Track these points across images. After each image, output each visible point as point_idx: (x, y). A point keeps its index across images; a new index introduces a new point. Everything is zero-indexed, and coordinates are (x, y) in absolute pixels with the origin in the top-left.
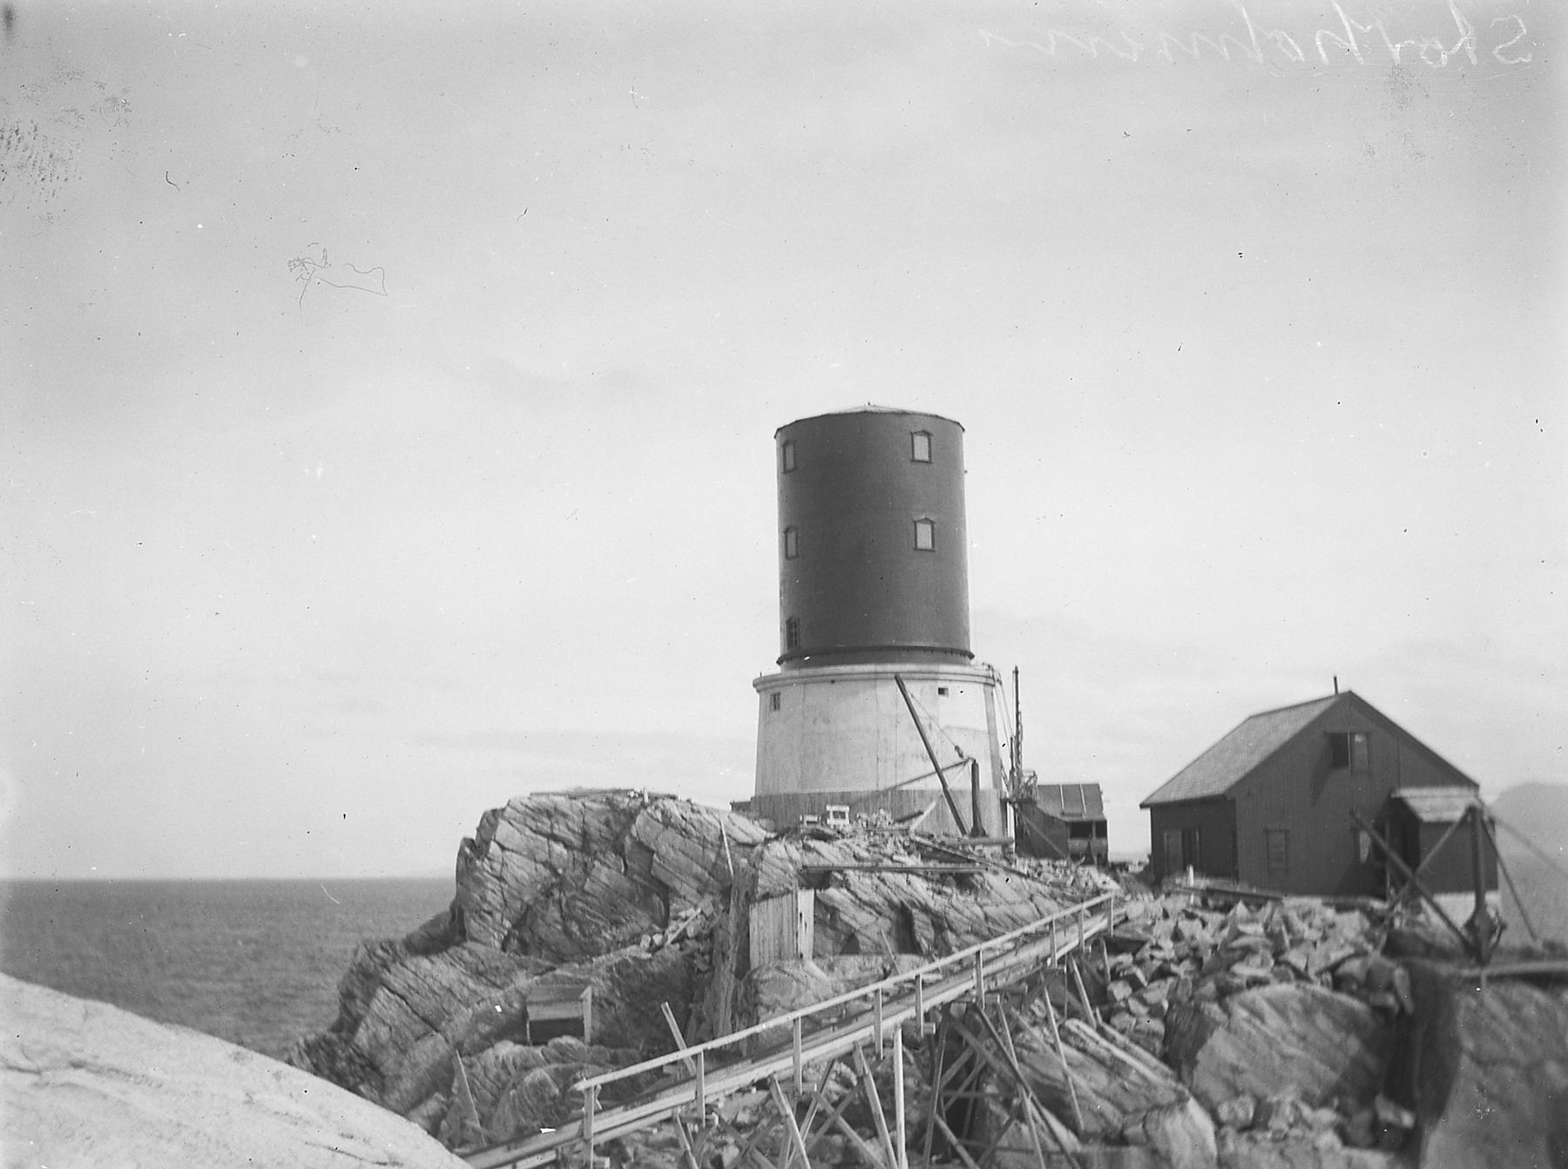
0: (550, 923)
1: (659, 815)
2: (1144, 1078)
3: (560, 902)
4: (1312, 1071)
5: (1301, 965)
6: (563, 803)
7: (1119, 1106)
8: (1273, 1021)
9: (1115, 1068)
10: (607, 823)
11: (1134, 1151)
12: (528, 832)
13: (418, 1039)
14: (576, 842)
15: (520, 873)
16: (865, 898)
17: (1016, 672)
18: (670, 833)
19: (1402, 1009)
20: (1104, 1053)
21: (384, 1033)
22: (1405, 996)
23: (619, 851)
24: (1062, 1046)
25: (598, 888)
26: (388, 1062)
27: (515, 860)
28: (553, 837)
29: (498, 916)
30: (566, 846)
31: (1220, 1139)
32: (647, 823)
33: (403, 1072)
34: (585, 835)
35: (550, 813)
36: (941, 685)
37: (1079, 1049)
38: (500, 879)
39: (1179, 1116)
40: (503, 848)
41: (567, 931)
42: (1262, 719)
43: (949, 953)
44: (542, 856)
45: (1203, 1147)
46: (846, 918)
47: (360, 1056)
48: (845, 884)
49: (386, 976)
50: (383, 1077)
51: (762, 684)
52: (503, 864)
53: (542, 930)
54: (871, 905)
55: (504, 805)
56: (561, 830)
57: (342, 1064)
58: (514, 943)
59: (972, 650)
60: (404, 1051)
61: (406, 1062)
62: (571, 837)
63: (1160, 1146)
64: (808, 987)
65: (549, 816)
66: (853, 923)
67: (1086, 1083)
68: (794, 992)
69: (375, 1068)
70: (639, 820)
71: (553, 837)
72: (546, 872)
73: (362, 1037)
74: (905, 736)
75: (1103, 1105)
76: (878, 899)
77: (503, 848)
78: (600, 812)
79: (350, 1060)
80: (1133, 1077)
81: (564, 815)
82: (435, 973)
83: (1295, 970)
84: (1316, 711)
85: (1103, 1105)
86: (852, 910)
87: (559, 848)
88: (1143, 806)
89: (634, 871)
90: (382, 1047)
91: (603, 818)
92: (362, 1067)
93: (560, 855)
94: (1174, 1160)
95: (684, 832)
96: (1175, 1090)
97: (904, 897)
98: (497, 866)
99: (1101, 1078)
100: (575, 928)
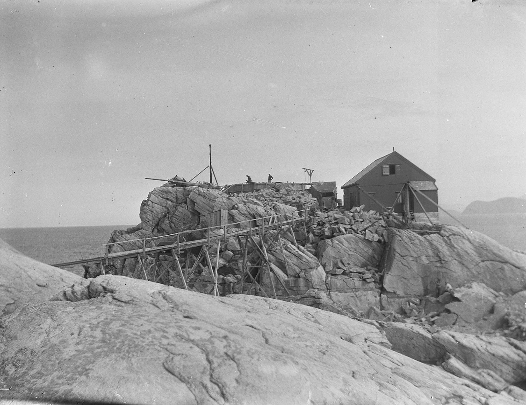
0: (166, 224)
1: (197, 192)
2: (307, 260)
3: (169, 218)
4: (358, 259)
5: (356, 229)
7: (299, 267)
8: (346, 244)
9: (299, 257)
11: (301, 279)
14: (175, 200)
15: (158, 210)
16: (242, 212)
17: (210, 146)
18: (200, 197)
19: (385, 241)
20: (296, 253)
22: (385, 237)
23: (186, 203)
24: (284, 251)
25: (179, 214)
28: (167, 199)
29: (151, 222)
31: (327, 277)
34: (177, 198)
37: (289, 252)
38: (152, 211)
39: (315, 270)
40: (153, 203)
41: (171, 226)
44: (164, 205)
45: (321, 278)
46: (237, 218)
48: (237, 209)
52: (153, 207)
53: (163, 226)
54: (244, 214)
56: (169, 197)
58: (156, 230)
62: (172, 199)
63: (309, 278)
65: (166, 193)
67: (291, 261)
70: (191, 193)
71: (167, 199)
75: (296, 268)
76: (246, 213)
77: (153, 203)
78: (181, 191)
80: (304, 260)
81: (171, 193)
83: (354, 230)
84: (385, 158)
85: (296, 268)
86: (238, 216)
87: (169, 202)
91: (182, 193)
94: (313, 282)
96: (316, 263)
97: (254, 212)
99: (295, 260)
100: (173, 225)
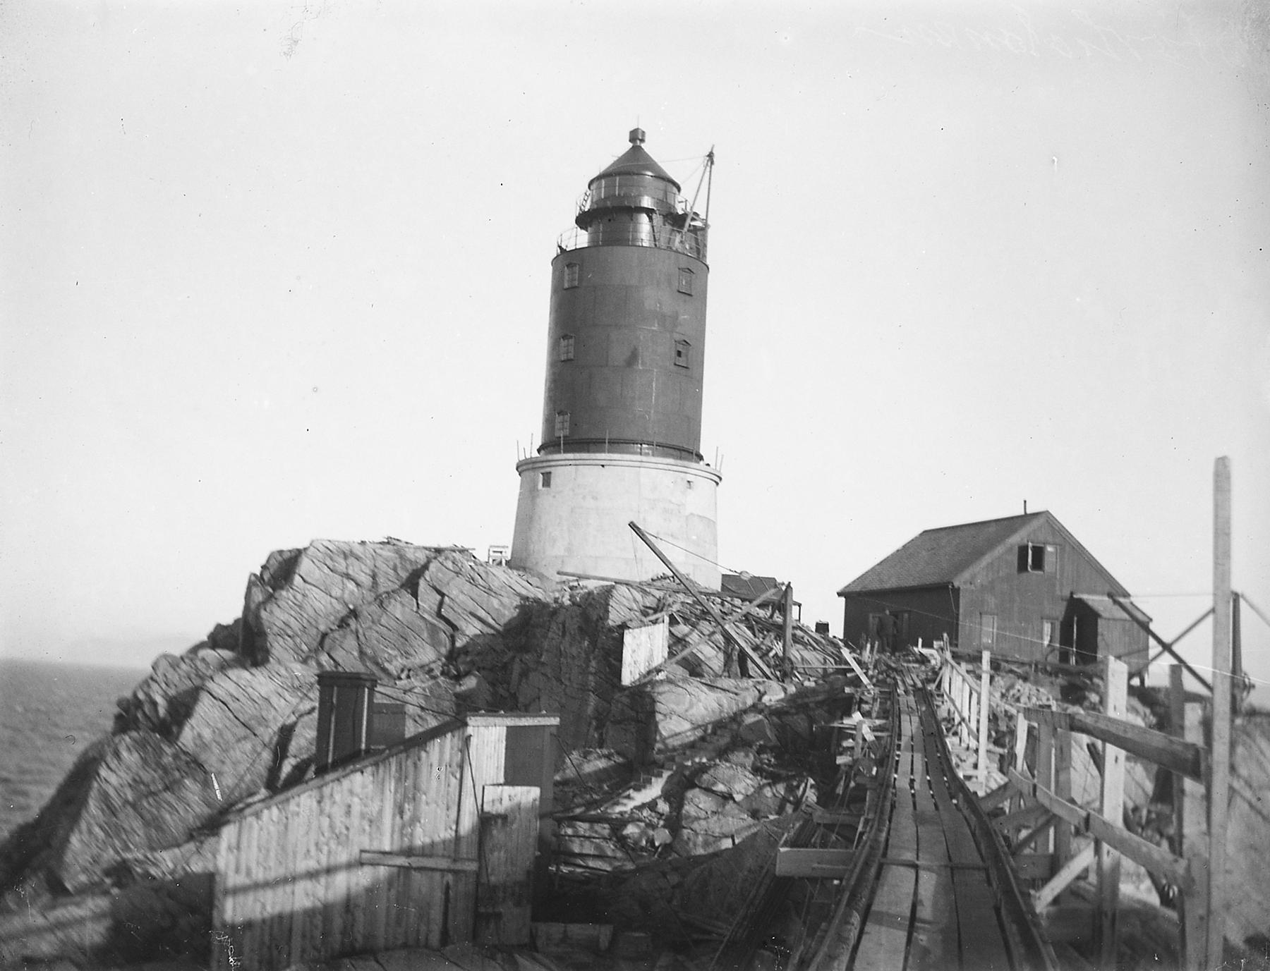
3: (357, 632)
6: (359, 550)
10: (395, 569)
12: (326, 570)
13: (239, 741)
18: (460, 581)
21: (207, 734)
26: (211, 760)
27: (314, 593)
30: (358, 584)
32: (439, 570)
33: (226, 769)
35: (347, 554)
36: (690, 478)
42: (943, 533)
43: (857, 677)
44: (336, 592)
47: (186, 753)
49: (210, 685)
50: (206, 772)
51: (524, 467)
55: (306, 544)
56: (356, 570)
57: (167, 760)
59: (702, 452)
60: (225, 751)
61: (228, 761)
64: (699, 701)
66: (699, 655)
68: (687, 705)
69: (200, 766)
72: (339, 607)
73: (187, 737)
74: (625, 527)
79: (176, 757)
81: (358, 558)
82: (254, 685)
88: (839, 594)
89: (424, 611)
90: (205, 746)
91: (391, 564)
92: (187, 763)
93: (352, 593)
95: (472, 581)
98: (299, 597)
